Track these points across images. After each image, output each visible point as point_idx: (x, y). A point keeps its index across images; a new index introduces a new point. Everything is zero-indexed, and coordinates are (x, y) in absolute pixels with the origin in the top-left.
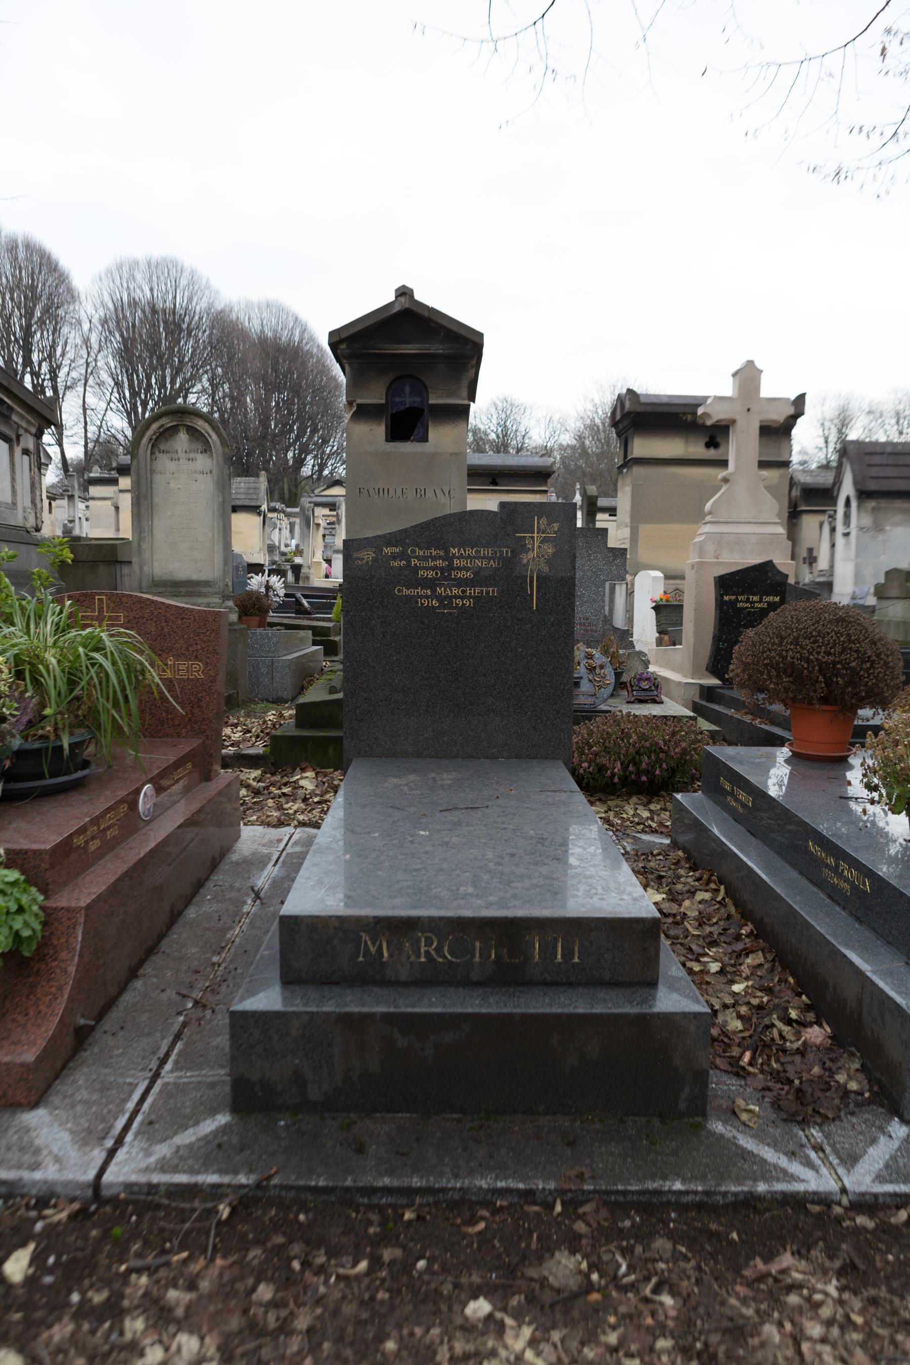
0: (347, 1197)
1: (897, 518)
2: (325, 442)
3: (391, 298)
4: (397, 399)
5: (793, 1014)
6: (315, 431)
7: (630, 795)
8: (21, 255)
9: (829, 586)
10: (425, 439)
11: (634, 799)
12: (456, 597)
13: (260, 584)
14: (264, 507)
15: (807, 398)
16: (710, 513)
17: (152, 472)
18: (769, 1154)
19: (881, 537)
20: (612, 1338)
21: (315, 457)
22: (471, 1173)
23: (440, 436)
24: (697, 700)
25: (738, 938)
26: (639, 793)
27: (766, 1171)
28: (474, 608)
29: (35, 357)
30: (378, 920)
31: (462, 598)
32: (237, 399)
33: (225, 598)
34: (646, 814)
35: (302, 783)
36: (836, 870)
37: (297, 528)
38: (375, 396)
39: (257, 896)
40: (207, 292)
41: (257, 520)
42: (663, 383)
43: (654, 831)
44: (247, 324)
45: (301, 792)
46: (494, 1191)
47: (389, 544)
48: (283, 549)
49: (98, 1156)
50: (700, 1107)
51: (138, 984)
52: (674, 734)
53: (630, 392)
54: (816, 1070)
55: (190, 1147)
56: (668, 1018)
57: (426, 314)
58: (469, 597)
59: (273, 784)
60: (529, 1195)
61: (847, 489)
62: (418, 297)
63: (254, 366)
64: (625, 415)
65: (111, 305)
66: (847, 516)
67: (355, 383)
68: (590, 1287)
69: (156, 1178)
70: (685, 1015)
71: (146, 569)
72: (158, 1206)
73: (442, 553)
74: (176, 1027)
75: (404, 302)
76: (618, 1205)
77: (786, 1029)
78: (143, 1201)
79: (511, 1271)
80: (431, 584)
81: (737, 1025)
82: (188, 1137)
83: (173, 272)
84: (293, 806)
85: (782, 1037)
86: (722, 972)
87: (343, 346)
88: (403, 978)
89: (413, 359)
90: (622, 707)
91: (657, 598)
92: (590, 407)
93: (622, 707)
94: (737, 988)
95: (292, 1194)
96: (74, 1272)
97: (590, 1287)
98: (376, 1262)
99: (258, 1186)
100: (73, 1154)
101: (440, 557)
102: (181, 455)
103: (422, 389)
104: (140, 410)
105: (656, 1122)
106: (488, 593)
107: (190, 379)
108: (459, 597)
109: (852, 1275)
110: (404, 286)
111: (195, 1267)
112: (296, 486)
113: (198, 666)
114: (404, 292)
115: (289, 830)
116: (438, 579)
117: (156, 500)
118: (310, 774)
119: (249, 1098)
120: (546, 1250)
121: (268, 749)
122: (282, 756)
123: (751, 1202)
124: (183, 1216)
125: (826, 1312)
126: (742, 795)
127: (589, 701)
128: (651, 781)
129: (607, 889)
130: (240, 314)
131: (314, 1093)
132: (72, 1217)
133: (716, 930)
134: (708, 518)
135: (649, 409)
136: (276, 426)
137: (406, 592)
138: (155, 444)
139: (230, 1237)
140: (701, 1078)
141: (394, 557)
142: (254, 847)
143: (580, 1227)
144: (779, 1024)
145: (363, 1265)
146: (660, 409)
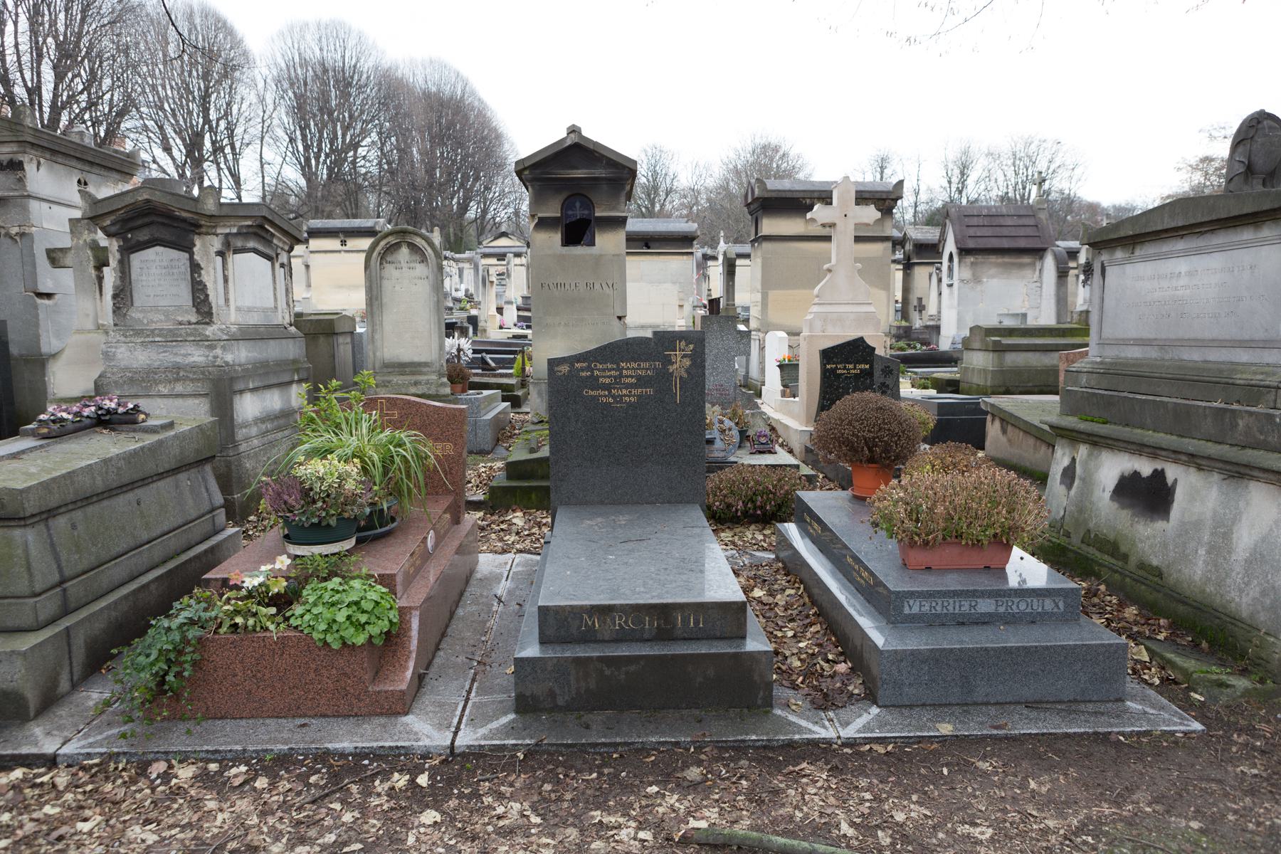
0: (583, 748)
1: (993, 271)
2: (487, 188)
4: (570, 212)
5: (830, 657)
6: (477, 179)
7: (750, 523)
8: (198, 21)
9: (937, 329)
10: (592, 243)
11: (753, 527)
13: (452, 346)
15: (906, 184)
17: (381, 278)
18: (803, 723)
19: (979, 288)
20: (717, 797)
21: (479, 203)
22: (647, 735)
25: (807, 616)
26: (756, 522)
27: (800, 729)
29: (213, 115)
30: (593, 607)
32: (404, 152)
33: (441, 375)
34: (761, 537)
35: (514, 521)
36: (858, 572)
37: (466, 272)
39: (500, 601)
43: (765, 550)
45: (514, 528)
46: (659, 743)
48: (455, 294)
49: (450, 736)
50: (769, 703)
51: (441, 653)
52: (779, 480)
54: (838, 685)
55: (497, 729)
56: (751, 654)
59: (493, 522)
60: (677, 744)
61: (950, 246)
63: (419, 119)
65: (283, 65)
66: (950, 269)
67: (535, 203)
68: (708, 780)
69: (483, 743)
70: (759, 652)
71: (378, 354)
72: (486, 755)
74: (471, 676)
75: (573, 138)
76: (722, 747)
77: (825, 665)
78: (477, 755)
79: (668, 775)
80: (608, 387)
81: (799, 664)
82: (495, 725)
83: (342, 35)
84: (511, 538)
85: (822, 669)
86: (794, 636)
87: (526, 172)
88: (607, 638)
90: (747, 459)
93: (747, 459)
94: (801, 645)
95: (554, 748)
96: (452, 782)
97: (708, 780)
98: (600, 774)
99: (537, 745)
100: (435, 734)
102: (404, 265)
103: (590, 205)
104: (313, 162)
105: (745, 711)
109: (834, 771)
111: (512, 778)
112: (462, 231)
113: (449, 446)
114: (574, 130)
115: (511, 556)
117: (385, 300)
118: (519, 514)
119: (525, 705)
120: (686, 766)
121: (487, 496)
122: (498, 501)
123: (791, 745)
124: (500, 758)
125: (819, 784)
126: (816, 526)
127: (722, 454)
128: (764, 514)
129: (719, 587)
130: (404, 71)
131: (560, 702)
132: (442, 762)
133: (795, 612)
134: (816, 300)
135: (774, 195)
136: (441, 176)
138: (383, 257)
139: (525, 765)
140: (769, 686)
141: (582, 370)
142: (490, 568)
143: (703, 757)
144: (822, 663)
145: (595, 775)
146: (784, 195)
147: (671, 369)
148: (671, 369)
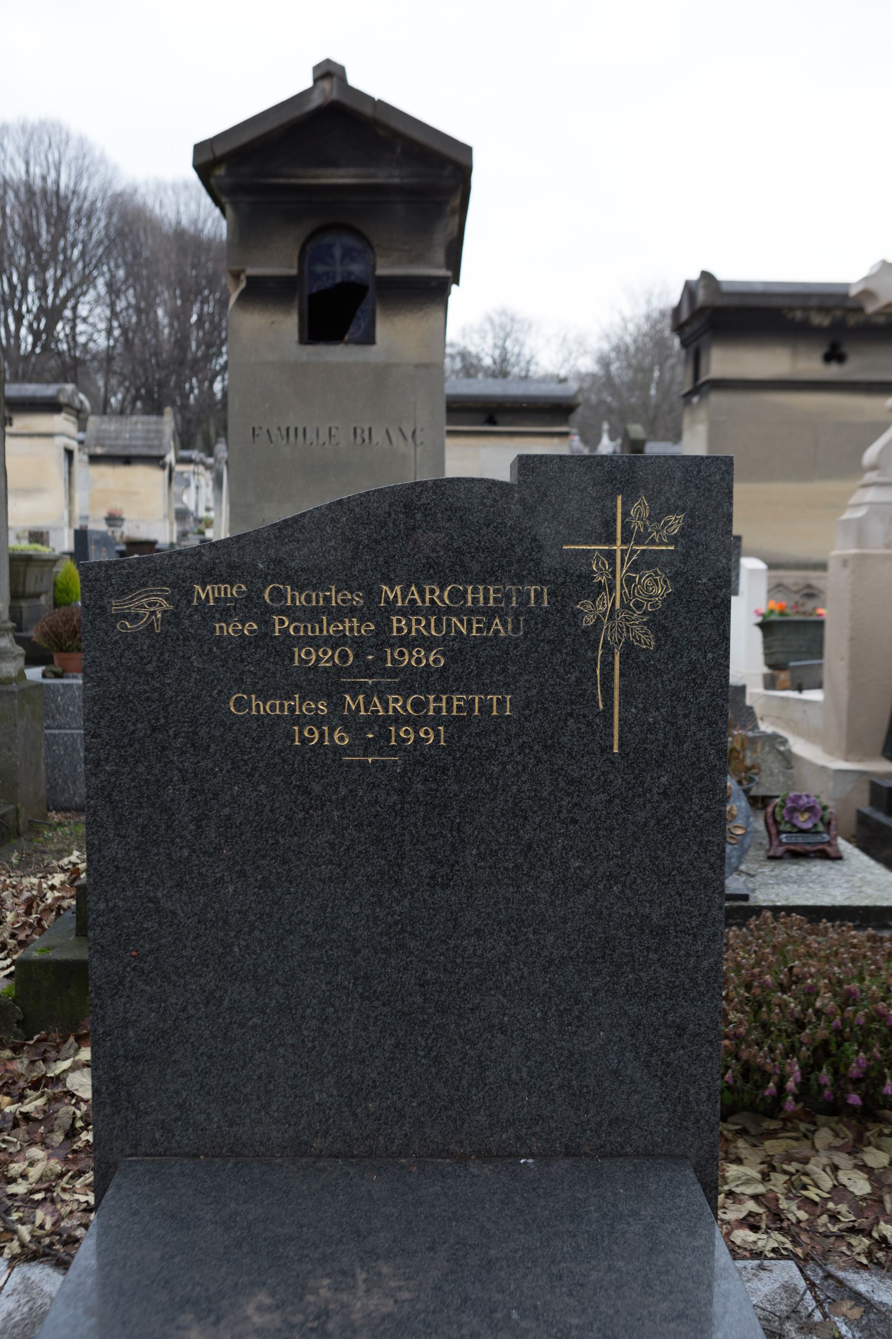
3: (305, 82)
4: (320, 268)
10: (369, 339)
12: (398, 720)
14: (170, 457)
16: (874, 467)
23: (395, 333)
24: (867, 809)
28: (449, 749)
31: (415, 723)
32: (145, 309)
38: (279, 261)
40: (102, 168)
41: (158, 476)
42: (757, 262)
44: (157, 210)
47: (208, 576)
53: (706, 276)
57: (368, 111)
58: (436, 721)
62: (354, 80)
64: (697, 313)
73: (358, 600)
80: (328, 684)
83: (56, 139)
87: (221, 171)
89: (343, 197)
91: (763, 609)
92: (617, 319)
101: (353, 611)
106: (486, 708)
107: (81, 284)
108: (408, 720)
110: (328, 62)
114: (328, 72)
116: (348, 672)
135: (735, 302)
136: (198, 347)
137: (260, 707)
141: (225, 611)
146: (753, 302)
147: (590, 612)
148: (590, 612)
